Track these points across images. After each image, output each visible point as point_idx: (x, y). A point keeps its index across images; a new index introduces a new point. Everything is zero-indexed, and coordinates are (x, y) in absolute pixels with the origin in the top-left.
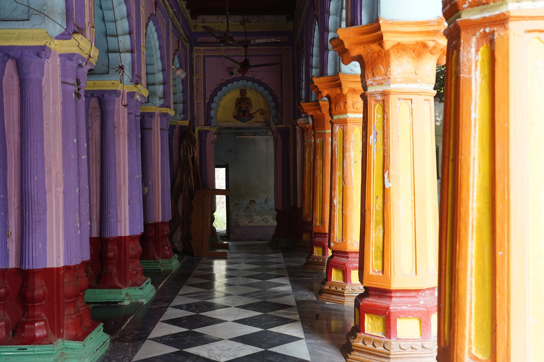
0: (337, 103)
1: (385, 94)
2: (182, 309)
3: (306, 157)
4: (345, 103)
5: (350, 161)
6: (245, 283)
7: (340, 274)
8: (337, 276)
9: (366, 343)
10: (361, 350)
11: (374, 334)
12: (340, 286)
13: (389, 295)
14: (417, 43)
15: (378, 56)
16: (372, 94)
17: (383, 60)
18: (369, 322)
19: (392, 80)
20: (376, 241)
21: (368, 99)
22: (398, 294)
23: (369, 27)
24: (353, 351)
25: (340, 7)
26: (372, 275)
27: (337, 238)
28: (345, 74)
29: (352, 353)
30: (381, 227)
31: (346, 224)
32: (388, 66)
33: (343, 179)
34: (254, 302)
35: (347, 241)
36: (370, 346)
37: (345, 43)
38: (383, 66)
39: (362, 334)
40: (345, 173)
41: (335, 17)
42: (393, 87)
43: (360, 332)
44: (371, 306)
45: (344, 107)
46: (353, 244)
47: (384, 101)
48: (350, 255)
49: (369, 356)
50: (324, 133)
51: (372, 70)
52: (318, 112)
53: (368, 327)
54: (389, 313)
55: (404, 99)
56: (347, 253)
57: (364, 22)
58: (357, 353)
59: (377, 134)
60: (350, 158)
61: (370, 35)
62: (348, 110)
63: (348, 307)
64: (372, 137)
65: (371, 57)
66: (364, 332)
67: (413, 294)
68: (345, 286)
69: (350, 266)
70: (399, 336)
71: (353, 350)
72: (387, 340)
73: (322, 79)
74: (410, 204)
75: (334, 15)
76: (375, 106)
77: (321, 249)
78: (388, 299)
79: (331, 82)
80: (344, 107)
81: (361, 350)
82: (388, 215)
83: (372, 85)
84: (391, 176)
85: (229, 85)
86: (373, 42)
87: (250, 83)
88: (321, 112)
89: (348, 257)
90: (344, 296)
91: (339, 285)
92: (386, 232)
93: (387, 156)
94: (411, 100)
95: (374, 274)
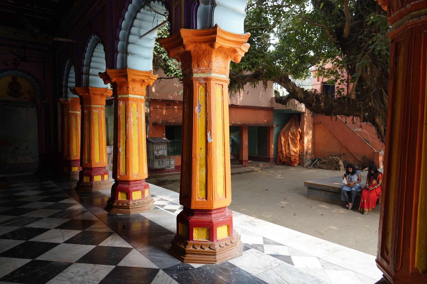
0: (121, 87)
1: (207, 80)
2: (8, 238)
3: (65, 121)
4: (128, 88)
5: (131, 124)
6: (45, 206)
7: (124, 195)
8: (122, 196)
9: (196, 247)
10: (192, 253)
11: (200, 240)
12: (125, 203)
13: (210, 213)
14: (231, 48)
15: (203, 53)
16: (198, 79)
17: (206, 56)
18: (196, 233)
19: (213, 70)
20: (200, 178)
21: (194, 82)
22: (215, 212)
23: (200, 32)
24: (186, 254)
25: (129, 25)
26: (198, 201)
27: (121, 173)
28: (131, 69)
29: (187, 255)
30: (204, 169)
31: (129, 164)
32: (210, 62)
33: (126, 135)
34: (65, 222)
35: (129, 174)
36: (199, 249)
37: (184, 40)
38: (206, 60)
39: (191, 241)
40: (127, 132)
41: (125, 31)
42: (213, 75)
43: (189, 240)
44: (198, 222)
45: (127, 90)
46: (133, 176)
47: (206, 84)
48: (131, 183)
49: (199, 256)
50: (91, 107)
51: (198, 62)
52: (87, 94)
53: (195, 236)
54: (213, 225)
55: (219, 84)
56: (129, 181)
57: (199, 27)
58: (190, 255)
59: (200, 106)
60: (131, 122)
61: (204, 37)
62: (130, 92)
63: (133, 215)
64: (197, 108)
65: (197, 53)
66: (192, 240)
67: (222, 210)
68: (129, 202)
69: (131, 189)
70: (218, 239)
71: (186, 254)
72: (211, 243)
73: (113, 71)
74: (222, 152)
75: (124, 30)
76: (199, 87)
77: (89, 178)
78: (208, 216)
79: (119, 73)
80: (127, 90)
81: (192, 253)
82: (210, 160)
83: (197, 72)
84: (212, 135)
85: (5, 73)
86: (205, 42)
87: (21, 73)
88: (89, 94)
89: (129, 184)
90: (129, 209)
91: (125, 202)
92: (209, 172)
93: (209, 121)
94: (222, 85)
95: (200, 200)
